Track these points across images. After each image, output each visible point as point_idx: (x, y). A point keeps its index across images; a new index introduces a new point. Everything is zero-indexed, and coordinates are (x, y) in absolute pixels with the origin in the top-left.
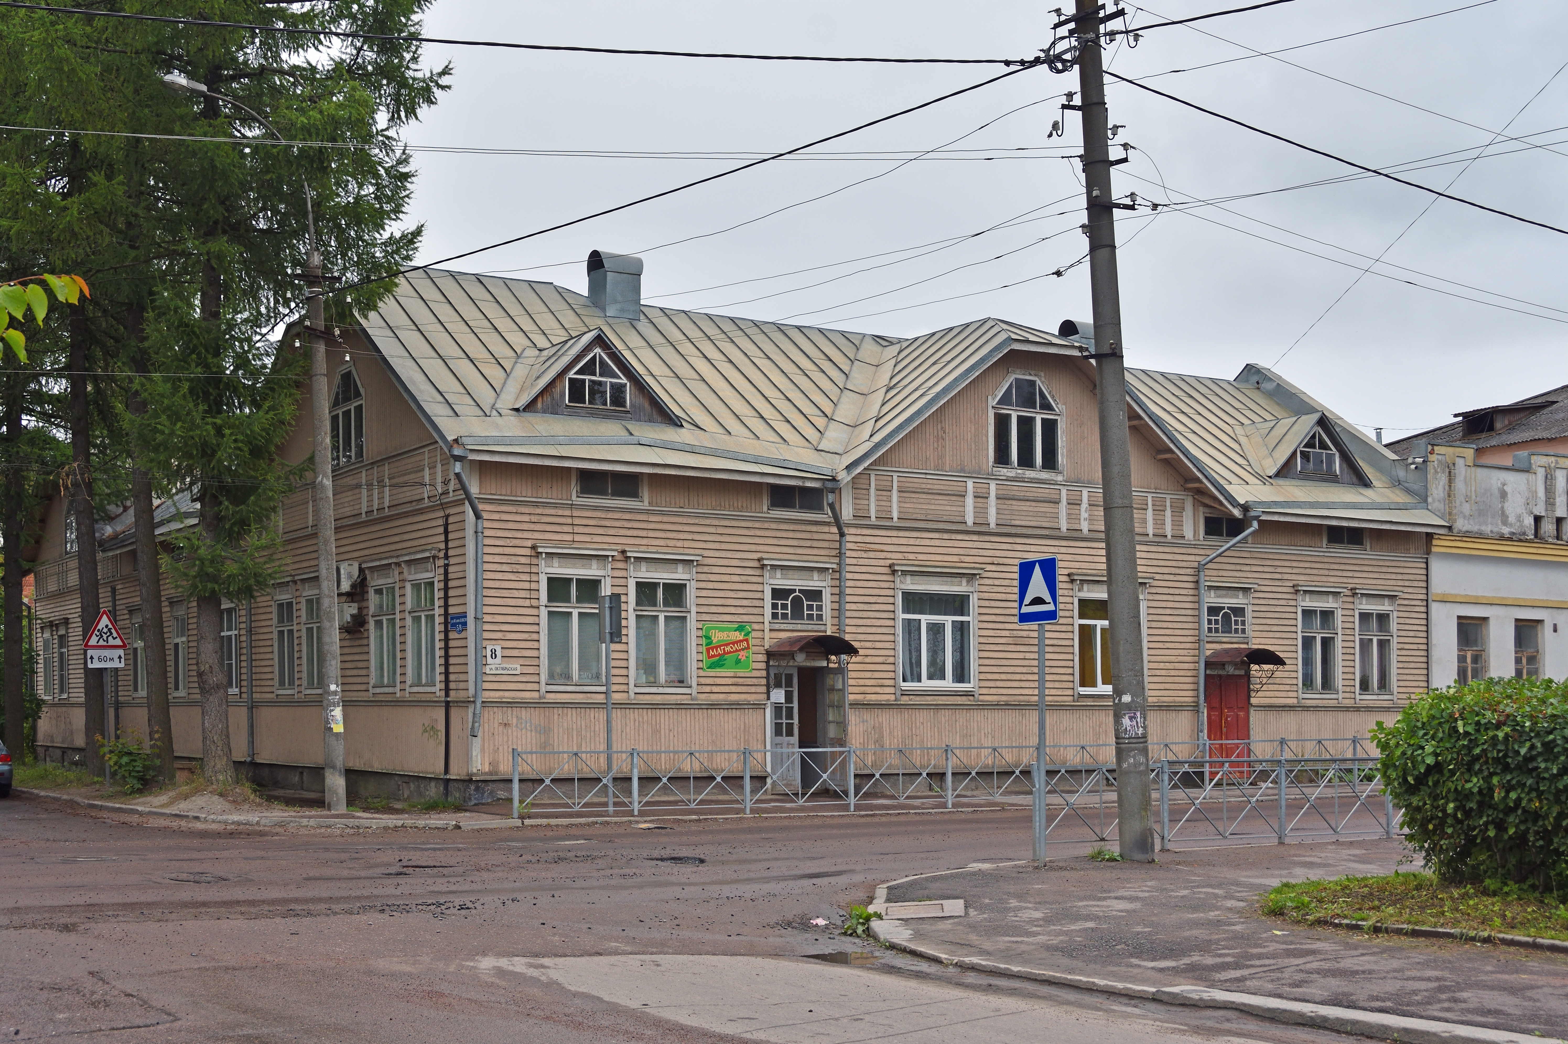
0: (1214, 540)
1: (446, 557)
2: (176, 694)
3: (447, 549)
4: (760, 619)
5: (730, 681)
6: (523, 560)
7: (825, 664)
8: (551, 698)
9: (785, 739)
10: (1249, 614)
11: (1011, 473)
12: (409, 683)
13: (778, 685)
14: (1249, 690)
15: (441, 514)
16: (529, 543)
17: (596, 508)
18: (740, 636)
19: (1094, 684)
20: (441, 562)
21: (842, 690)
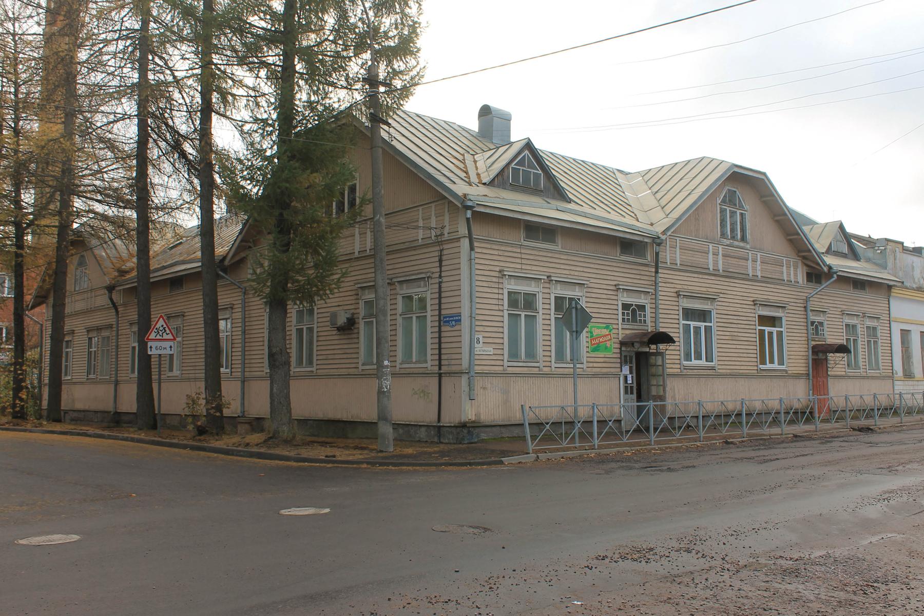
0: (811, 285)
1: (440, 277)
2: (170, 374)
3: (441, 272)
4: (616, 322)
5: (602, 360)
6: (495, 280)
7: (647, 350)
8: (510, 370)
9: (630, 396)
10: (825, 323)
11: (728, 242)
12: (399, 361)
13: (626, 362)
14: (827, 368)
15: (438, 248)
16: (498, 269)
17: (533, 248)
18: (606, 332)
19: (765, 364)
20: (437, 281)
21: (663, 366)
